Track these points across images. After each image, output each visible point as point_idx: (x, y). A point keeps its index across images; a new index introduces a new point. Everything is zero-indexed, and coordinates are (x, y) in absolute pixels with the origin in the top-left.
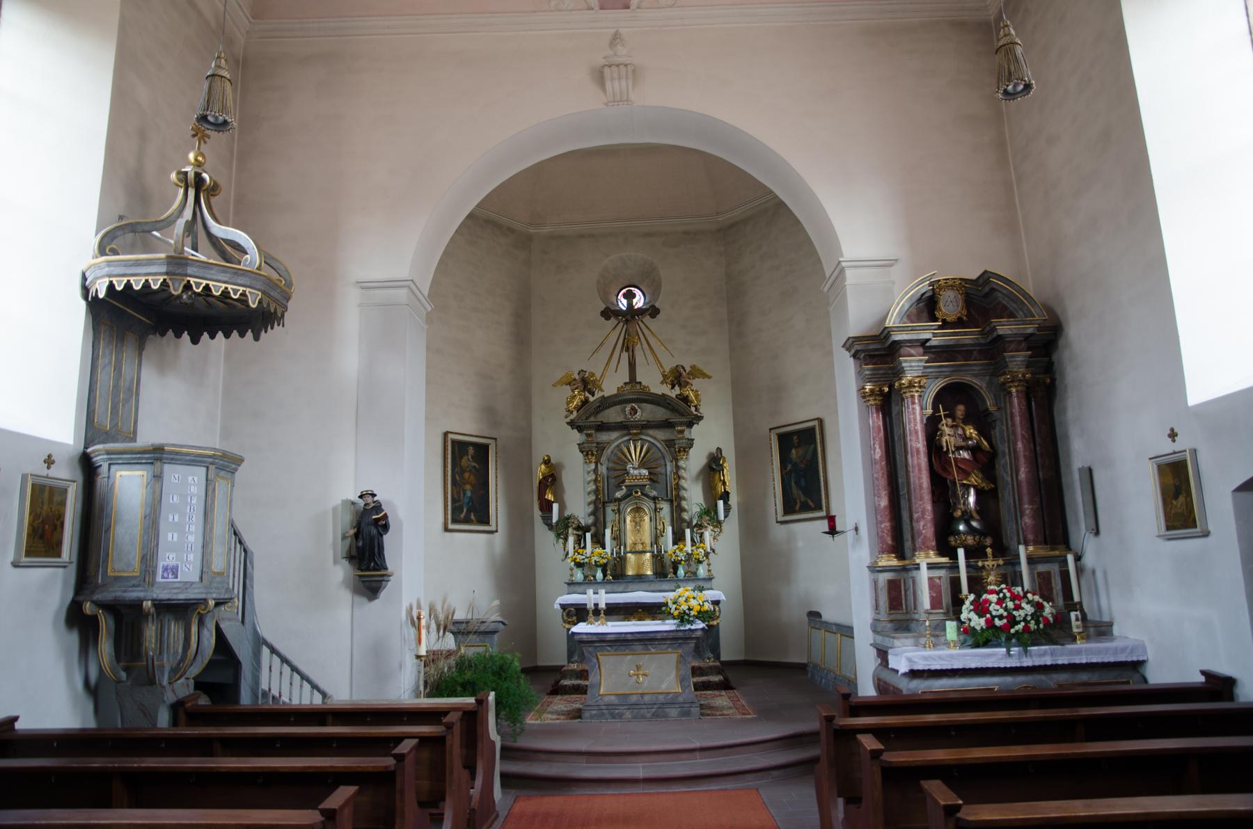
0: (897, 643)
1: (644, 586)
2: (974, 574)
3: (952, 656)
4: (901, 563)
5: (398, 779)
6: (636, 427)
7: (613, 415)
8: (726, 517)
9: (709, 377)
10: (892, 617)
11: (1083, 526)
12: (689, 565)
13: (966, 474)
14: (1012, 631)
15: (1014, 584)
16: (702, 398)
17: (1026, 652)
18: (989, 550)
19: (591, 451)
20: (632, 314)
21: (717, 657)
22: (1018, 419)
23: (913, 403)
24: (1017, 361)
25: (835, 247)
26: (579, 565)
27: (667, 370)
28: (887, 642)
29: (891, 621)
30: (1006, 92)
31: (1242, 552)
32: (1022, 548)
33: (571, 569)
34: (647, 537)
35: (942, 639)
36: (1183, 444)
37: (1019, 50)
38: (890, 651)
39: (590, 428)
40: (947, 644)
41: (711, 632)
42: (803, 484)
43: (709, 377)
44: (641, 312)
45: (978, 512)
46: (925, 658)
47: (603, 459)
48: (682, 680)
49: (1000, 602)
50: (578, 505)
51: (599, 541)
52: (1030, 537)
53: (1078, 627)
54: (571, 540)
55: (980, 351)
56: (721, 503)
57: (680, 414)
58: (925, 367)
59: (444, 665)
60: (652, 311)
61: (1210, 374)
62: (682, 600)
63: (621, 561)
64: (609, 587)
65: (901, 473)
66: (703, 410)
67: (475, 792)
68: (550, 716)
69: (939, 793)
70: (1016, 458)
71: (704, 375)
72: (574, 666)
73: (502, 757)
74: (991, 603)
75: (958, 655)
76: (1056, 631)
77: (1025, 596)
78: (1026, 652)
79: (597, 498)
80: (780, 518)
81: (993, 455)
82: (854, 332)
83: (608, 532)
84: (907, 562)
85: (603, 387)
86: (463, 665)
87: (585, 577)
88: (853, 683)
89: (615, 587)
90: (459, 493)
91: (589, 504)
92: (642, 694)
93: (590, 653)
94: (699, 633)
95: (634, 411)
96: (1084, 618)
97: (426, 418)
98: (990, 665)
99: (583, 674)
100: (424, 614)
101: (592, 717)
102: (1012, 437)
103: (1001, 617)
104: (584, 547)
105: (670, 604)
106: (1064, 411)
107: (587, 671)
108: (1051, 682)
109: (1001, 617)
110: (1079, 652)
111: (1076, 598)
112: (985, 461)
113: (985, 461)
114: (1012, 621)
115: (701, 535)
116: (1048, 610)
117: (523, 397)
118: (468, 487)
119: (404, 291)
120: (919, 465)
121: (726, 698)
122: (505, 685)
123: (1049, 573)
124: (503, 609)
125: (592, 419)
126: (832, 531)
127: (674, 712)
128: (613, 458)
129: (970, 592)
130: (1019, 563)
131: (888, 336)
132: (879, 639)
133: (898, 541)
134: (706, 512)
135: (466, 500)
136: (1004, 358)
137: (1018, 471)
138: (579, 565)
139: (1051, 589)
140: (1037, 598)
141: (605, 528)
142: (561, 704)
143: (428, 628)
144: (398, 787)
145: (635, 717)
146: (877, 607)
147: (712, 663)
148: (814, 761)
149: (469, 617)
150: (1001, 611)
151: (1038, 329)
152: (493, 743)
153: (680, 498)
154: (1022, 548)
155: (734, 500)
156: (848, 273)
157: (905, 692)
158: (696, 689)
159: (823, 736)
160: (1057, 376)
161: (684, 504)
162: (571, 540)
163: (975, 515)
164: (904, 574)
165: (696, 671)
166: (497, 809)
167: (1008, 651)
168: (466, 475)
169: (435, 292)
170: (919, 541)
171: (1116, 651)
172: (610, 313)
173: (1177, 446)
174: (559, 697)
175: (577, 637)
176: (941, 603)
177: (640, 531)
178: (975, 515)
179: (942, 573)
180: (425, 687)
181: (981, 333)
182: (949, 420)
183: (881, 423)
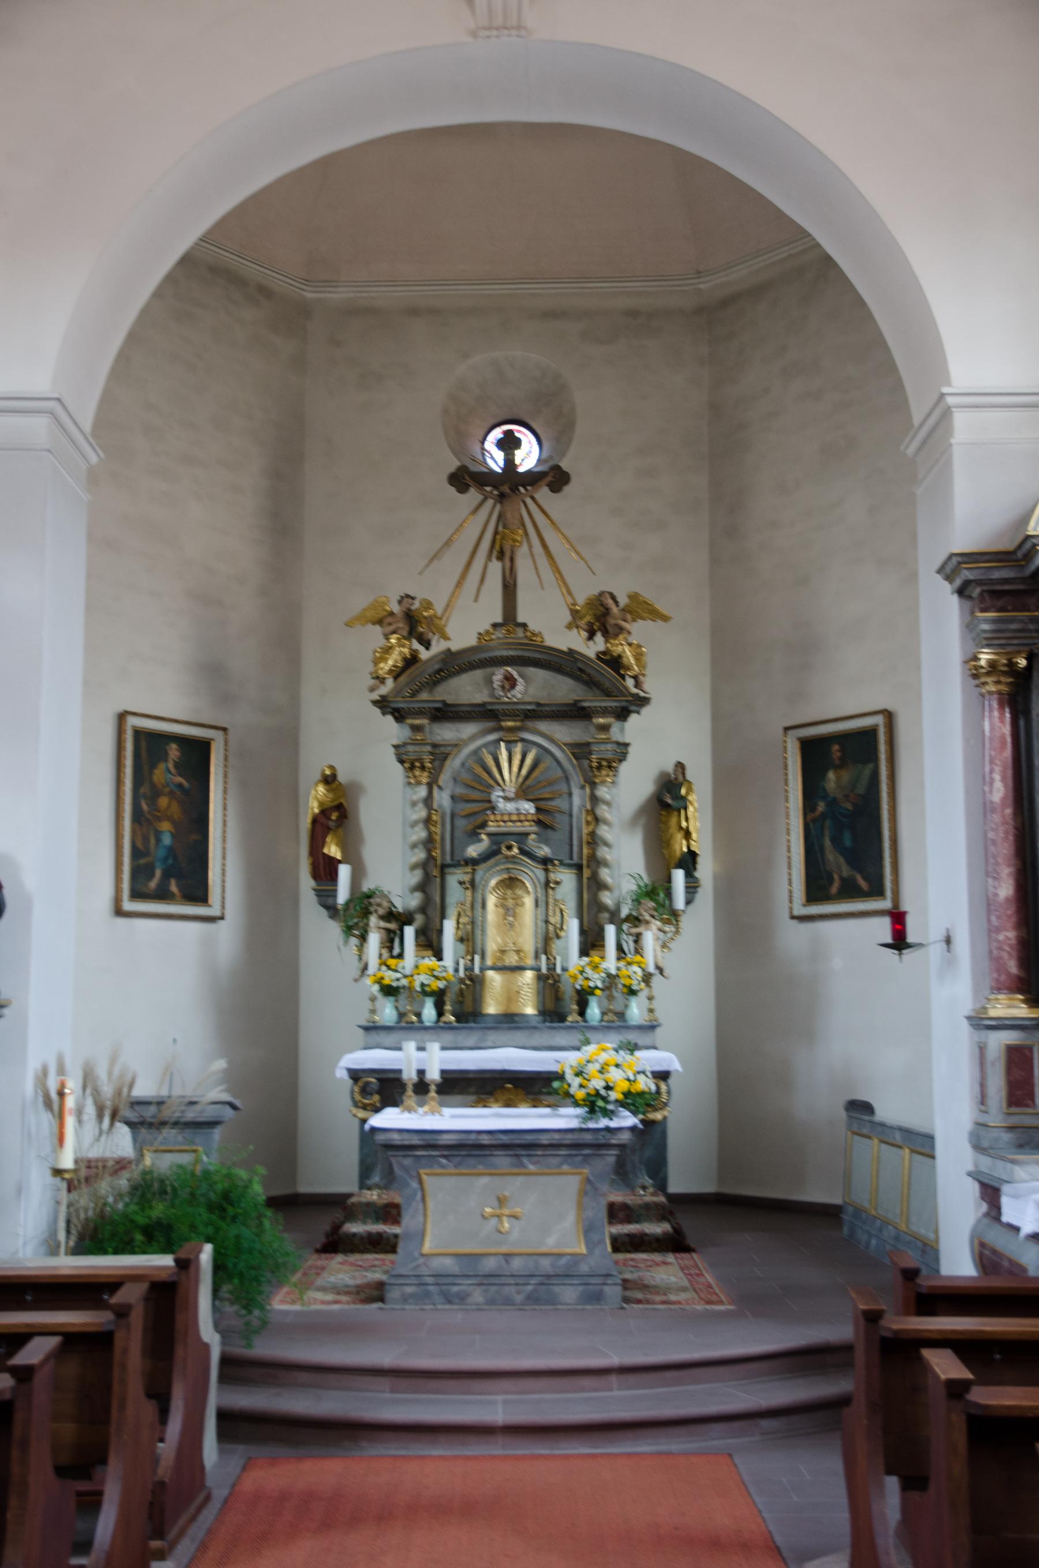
0: (1020, 1172)
1: (520, 1036)
5: (19, 1416)
6: (512, 715)
7: (466, 689)
8: (688, 902)
9: (665, 619)
10: (1015, 1120)
12: (611, 998)
16: (648, 659)
19: (420, 762)
20: (510, 484)
21: (661, 1185)
25: (936, 364)
26: (389, 991)
27: (581, 600)
28: (998, 1169)
29: (1011, 1128)
33: (373, 999)
34: (527, 939)
38: (1005, 1189)
39: (419, 713)
41: (651, 1133)
43: (665, 619)
44: (532, 478)
47: (444, 778)
48: (588, 1230)
50: (389, 865)
51: (430, 942)
54: (374, 939)
56: (679, 876)
57: (604, 691)
59: (111, 1190)
60: (554, 477)
62: (592, 1069)
63: (474, 984)
64: (448, 1037)
66: (650, 686)
67: (167, 1449)
68: (319, 1296)
72: (373, 1196)
73: (223, 1379)
79: (430, 858)
80: (800, 910)
83: (449, 927)
85: (449, 630)
86: (146, 1189)
87: (401, 1015)
88: (930, 1250)
89: (462, 1038)
90: (146, 839)
91: (414, 867)
92: (508, 1256)
93: (406, 1169)
94: (625, 1137)
95: (510, 682)
97: (86, 683)
99: (390, 1213)
100: (73, 1086)
101: (405, 1299)
104: (401, 956)
105: (569, 1076)
107: (397, 1206)
115: (638, 939)
117: (285, 645)
118: (165, 826)
119: (41, 423)
121: (677, 1268)
122: (233, 1230)
124: (231, 1078)
125: (424, 696)
126: (899, 942)
127: (569, 1293)
128: (466, 776)
132: (986, 1163)
134: (650, 893)
135: (161, 853)
138: (389, 991)
141: (443, 916)
142: (343, 1271)
143: (79, 1112)
144: (17, 1431)
145: (491, 1302)
146: (983, 1099)
147: (649, 1196)
148: (842, 1402)
149: (164, 1092)
152: (206, 1347)
153: (596, 862)
155: (705, 870)
156: (959, 419)
158: (616, 1249)
159: (860, 1356)
161: (605, 874)
162: (374, 939)
165: (616, 1213)
166: (209, 1482)
168: (163, 802)
169: (107, 423)
172: (465, 478)
174: (340, 1258)
175: (380, 1138)
177: (513, 925)
180: (68, 1232)
183: (1007, 730)
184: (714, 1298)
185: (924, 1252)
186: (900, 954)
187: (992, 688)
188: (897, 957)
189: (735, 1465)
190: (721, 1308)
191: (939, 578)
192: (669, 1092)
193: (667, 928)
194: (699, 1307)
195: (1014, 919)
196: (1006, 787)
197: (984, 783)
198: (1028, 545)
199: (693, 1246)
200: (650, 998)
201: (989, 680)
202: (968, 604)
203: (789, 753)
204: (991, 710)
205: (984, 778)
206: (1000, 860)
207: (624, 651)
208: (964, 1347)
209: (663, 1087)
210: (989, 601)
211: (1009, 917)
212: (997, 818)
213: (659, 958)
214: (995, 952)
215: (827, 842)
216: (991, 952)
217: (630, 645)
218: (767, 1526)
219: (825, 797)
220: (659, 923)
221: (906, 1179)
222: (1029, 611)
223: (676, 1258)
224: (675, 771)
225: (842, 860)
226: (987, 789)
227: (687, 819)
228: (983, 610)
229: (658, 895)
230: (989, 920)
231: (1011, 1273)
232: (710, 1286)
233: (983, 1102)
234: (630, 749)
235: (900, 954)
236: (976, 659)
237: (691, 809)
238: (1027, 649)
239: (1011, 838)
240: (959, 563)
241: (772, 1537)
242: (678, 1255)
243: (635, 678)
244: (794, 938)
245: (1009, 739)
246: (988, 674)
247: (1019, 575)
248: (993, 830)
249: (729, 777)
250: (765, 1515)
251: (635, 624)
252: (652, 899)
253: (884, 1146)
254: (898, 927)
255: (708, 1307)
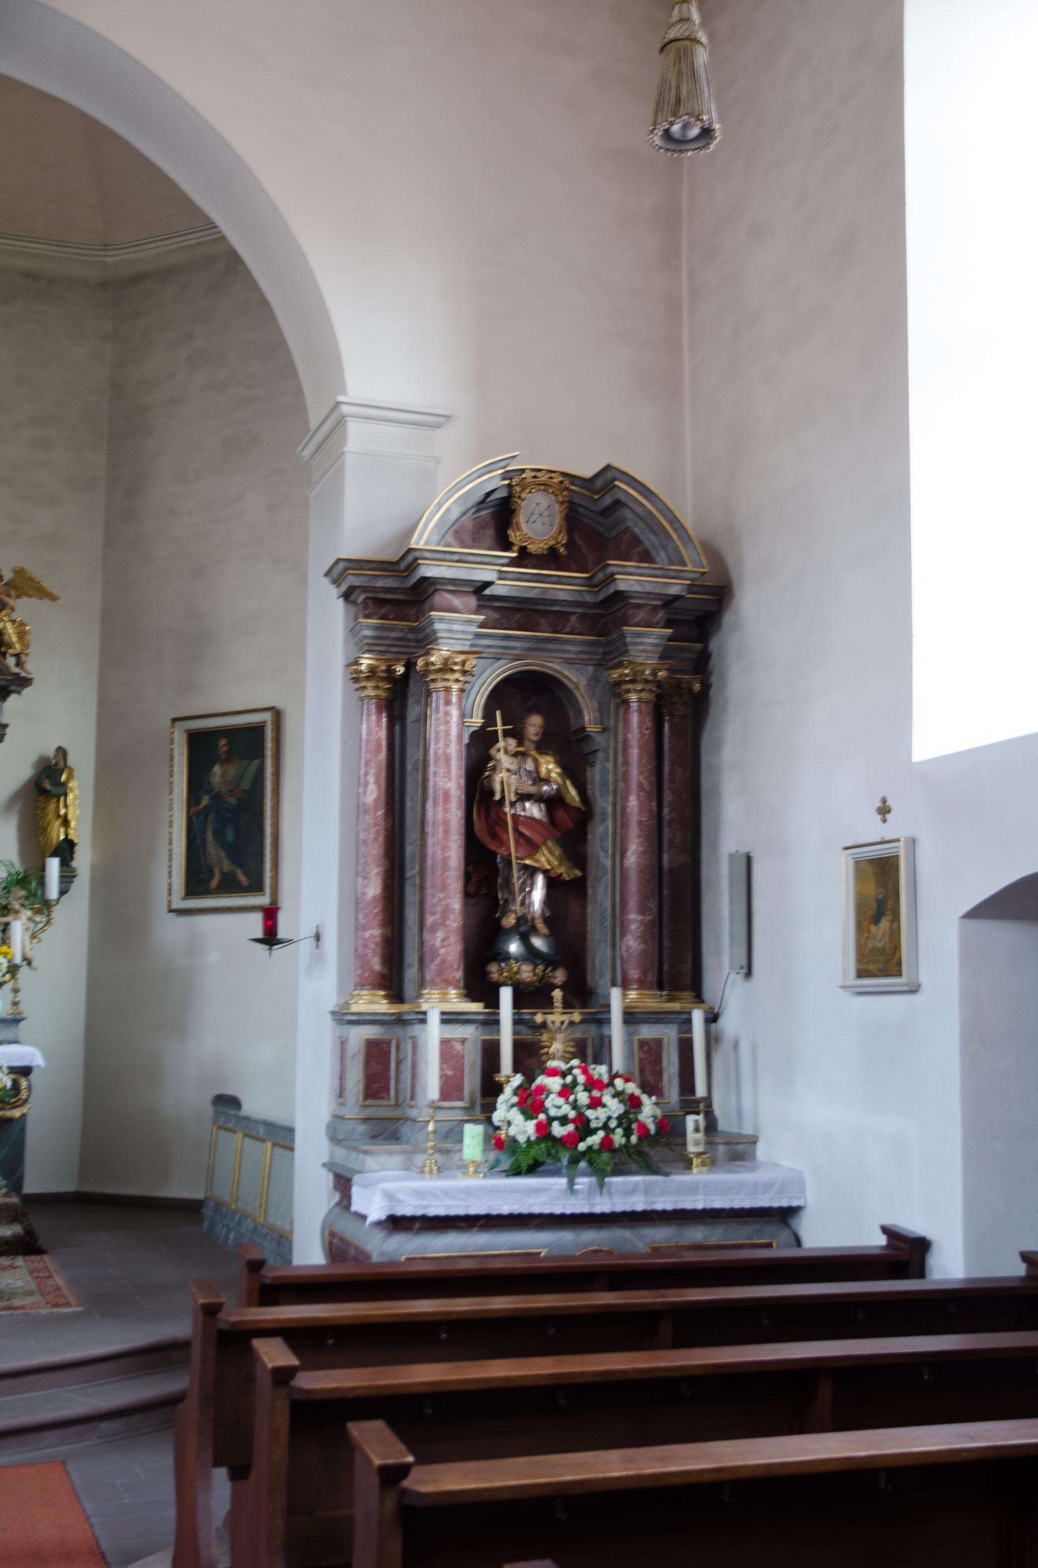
0: (371, 1162)
2: (527, 1036)
3: (468, 1191)
4: (395, 1009)
8: (63, 892)
9: (53, 598)
10: (370, 1112)
11: (726, 960)
13: (533, 847)
14: (582, 1146)
15: (597, 1061)
17: (601, 1185)
18: (557, 994)
21: (16, 1185)
22: (634, 752)
23: (448, 703)
24: (646, 644)
29: (366, 1120)
30: (667, 135)
31: (964, 1023)
32: (615, 993)
35: (456, 1157)
36: (896, 827)
37: (702, 57)
38: (356, 1179)
40: (463, 1167)
42: (230, 836)
43: (53, 598)
45: (547, 921)
46: (419, 1194)
49: (566, 1092)
52: (634, 974)
53: (697, 1143)
55: (582, 617)
56: (53, 865)
58: (478, 636)
61: (952, 713)
65: (412, 835)
66: (33, 667)
69: (376, 1444)
70: (625, 825)
71: (41, 592)
74: (550, 1093)
75: (482, 1189)
76: (655, 1148)
77: (611, 1084)
78: (601, 1185)
80: (178, 903)
81: (585, 816)
82: (352, 548)
84: (405, 1007)
88: (284, 1241)
96: (711, 1127)
98: (536, 1210)
102: (621, 786)
103: (564, 1120)
106: (718, 746)
108: (640, 1242)
109: (564, 1120)
110: (693, 1189)
111: (701, 1091)
112: (570, 826)
113: (570, 826)
114: (584, 1128)
116: (649, 1111)
120: (446, 822)
121: (24, 1272)
123: (659, 1043)
126: (270, 937)
129: (516, 1071)
130: (608, 1021)
131: (413, 566)
132: (340, 1153)
133: (393, 971)
134: (22, 881)
136: (623, 636)
137: (624, 849)
139: (659, 1073)
140: (632, 1088)
150: (567, 1110)
151: (691, 588)
154: (615, 993)
155: (83, 859)
156: (353, 428)
157: (375, 1258)
160: (714, 680)
163: (540, 925)
164: (398, 1031)
167: (571, 1183)
170: (431, 969)
171: (755, 1188)
173: (888, 831)
176: (460, 1088)
178: (540, 925)
179: (469, 1032)
181: (589, 583)
182: (512, 743)
183: (383, 734)
184: (62, 1300)
185: (279, 1243)
186: (270, 949)
187: (371, 692)
188: (267, 952)
189: (67, 1473)
190: (68, 1310)
191: (326, 581)
192: (29, 1088)
193: (38, 918)
194: (44, 1311)
195: (380, 918)
196: (379, 788)
197: (359, 785)
198: (410, 558)
199: (44, 1247)
200: (16, 991)
201: (369, 684)
202: (353, 609)
203: (176, 745)
204: (369, 715)
205: (359, 779)
206: (370, 860)
207: (5, 628)
208: (295, 1335)
209: (24, 1083)
210: (371, 609)
211: (376, 914)
212: (369, 818)
213: (28, 949)
214: (360, 949)
215: (210, 836)
216: (356, 949)
217: (14, 621)
218: (93, 1532)
219: (210, 791)
220: (29, 913)
221: (267, 1172)
222: (409, 621)
223: (26, 1261)
224: (56, 756)
225: (223, 855)
226: (361, 790)
227: (66, 806)
228: (367, 617)
229: (30, 883)
230: (356, 918)
231: (356, 1260)
232: (58, 1289)
233: (341, 1095)
234: (8, 730)
235: (270, 949)
236: (356, 663)
237: (71, 796)
238: (406, 657)
239: (381, 839)
240: (346, 569)
241: (97, 1543)
242: (28, 1258)
243: (17, 656)
244: (171, 932)
245: (384, 743)
246: (368, 678)
247: (402, 586)
248: (365, 830)
249: (111, 766)
250: (93, 1520)
251: (19, 601)
252: (23, 888)
253: (247, 1140)
254: (270, 923)
255: (55, 1310)
